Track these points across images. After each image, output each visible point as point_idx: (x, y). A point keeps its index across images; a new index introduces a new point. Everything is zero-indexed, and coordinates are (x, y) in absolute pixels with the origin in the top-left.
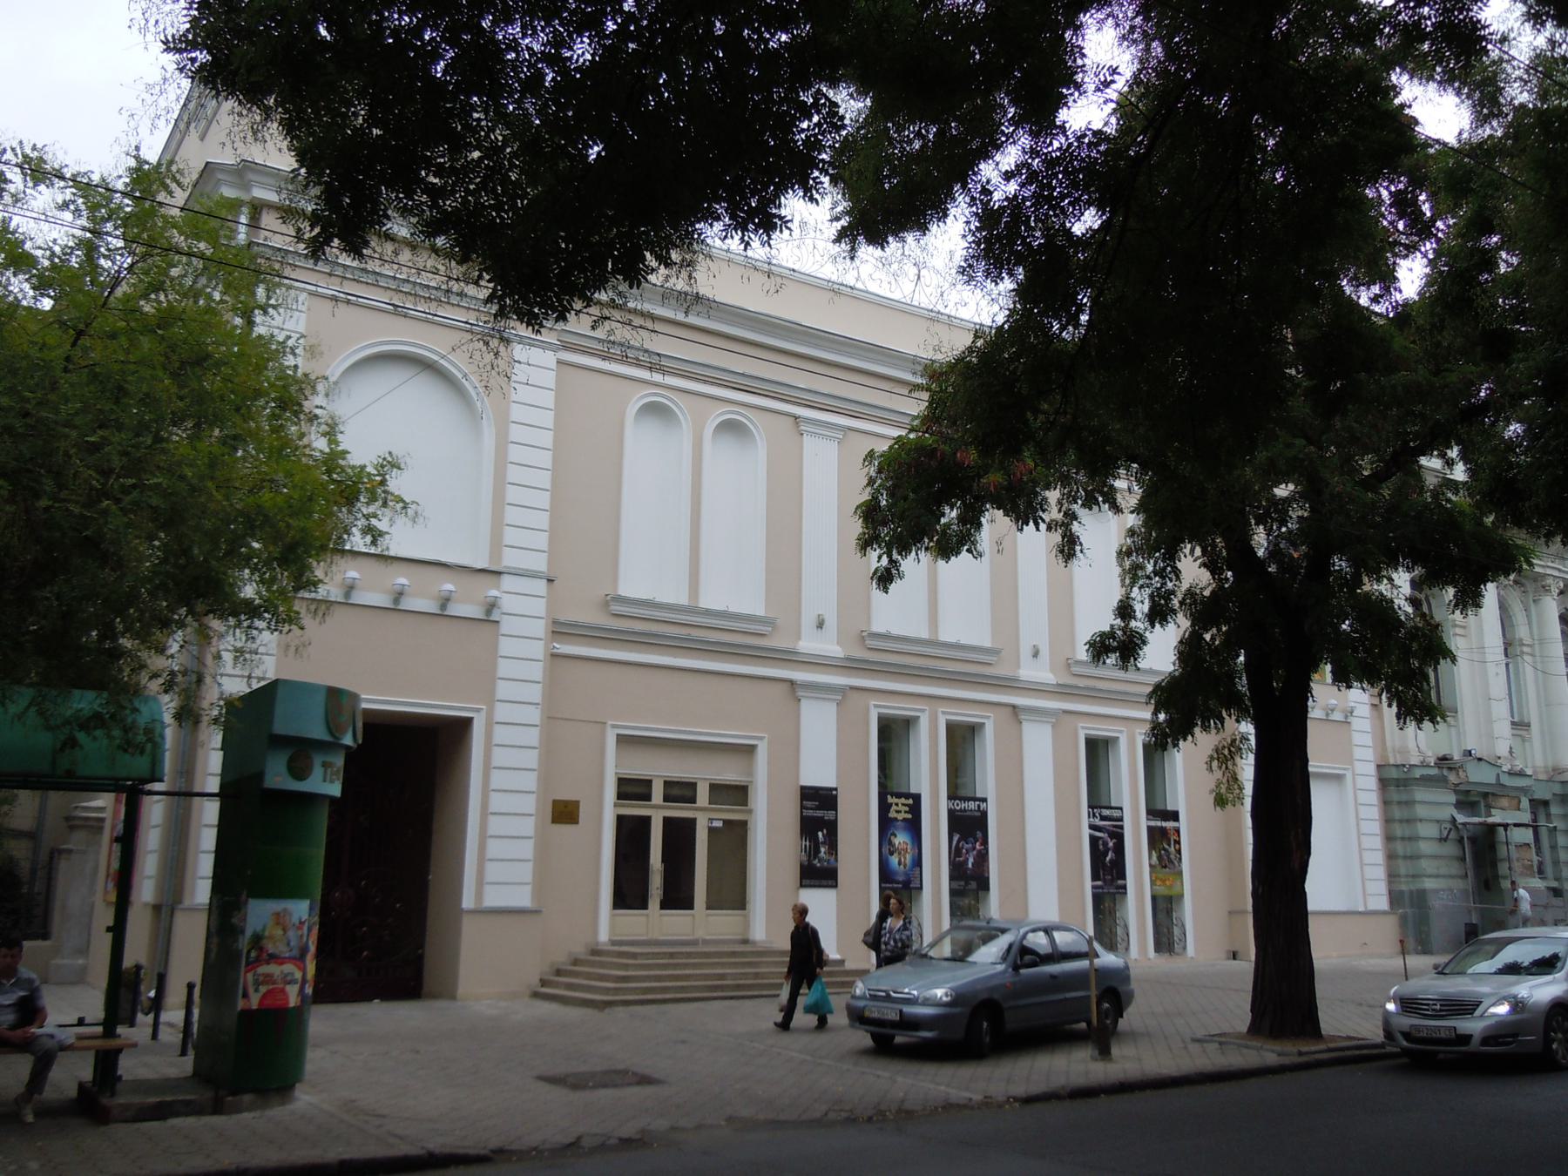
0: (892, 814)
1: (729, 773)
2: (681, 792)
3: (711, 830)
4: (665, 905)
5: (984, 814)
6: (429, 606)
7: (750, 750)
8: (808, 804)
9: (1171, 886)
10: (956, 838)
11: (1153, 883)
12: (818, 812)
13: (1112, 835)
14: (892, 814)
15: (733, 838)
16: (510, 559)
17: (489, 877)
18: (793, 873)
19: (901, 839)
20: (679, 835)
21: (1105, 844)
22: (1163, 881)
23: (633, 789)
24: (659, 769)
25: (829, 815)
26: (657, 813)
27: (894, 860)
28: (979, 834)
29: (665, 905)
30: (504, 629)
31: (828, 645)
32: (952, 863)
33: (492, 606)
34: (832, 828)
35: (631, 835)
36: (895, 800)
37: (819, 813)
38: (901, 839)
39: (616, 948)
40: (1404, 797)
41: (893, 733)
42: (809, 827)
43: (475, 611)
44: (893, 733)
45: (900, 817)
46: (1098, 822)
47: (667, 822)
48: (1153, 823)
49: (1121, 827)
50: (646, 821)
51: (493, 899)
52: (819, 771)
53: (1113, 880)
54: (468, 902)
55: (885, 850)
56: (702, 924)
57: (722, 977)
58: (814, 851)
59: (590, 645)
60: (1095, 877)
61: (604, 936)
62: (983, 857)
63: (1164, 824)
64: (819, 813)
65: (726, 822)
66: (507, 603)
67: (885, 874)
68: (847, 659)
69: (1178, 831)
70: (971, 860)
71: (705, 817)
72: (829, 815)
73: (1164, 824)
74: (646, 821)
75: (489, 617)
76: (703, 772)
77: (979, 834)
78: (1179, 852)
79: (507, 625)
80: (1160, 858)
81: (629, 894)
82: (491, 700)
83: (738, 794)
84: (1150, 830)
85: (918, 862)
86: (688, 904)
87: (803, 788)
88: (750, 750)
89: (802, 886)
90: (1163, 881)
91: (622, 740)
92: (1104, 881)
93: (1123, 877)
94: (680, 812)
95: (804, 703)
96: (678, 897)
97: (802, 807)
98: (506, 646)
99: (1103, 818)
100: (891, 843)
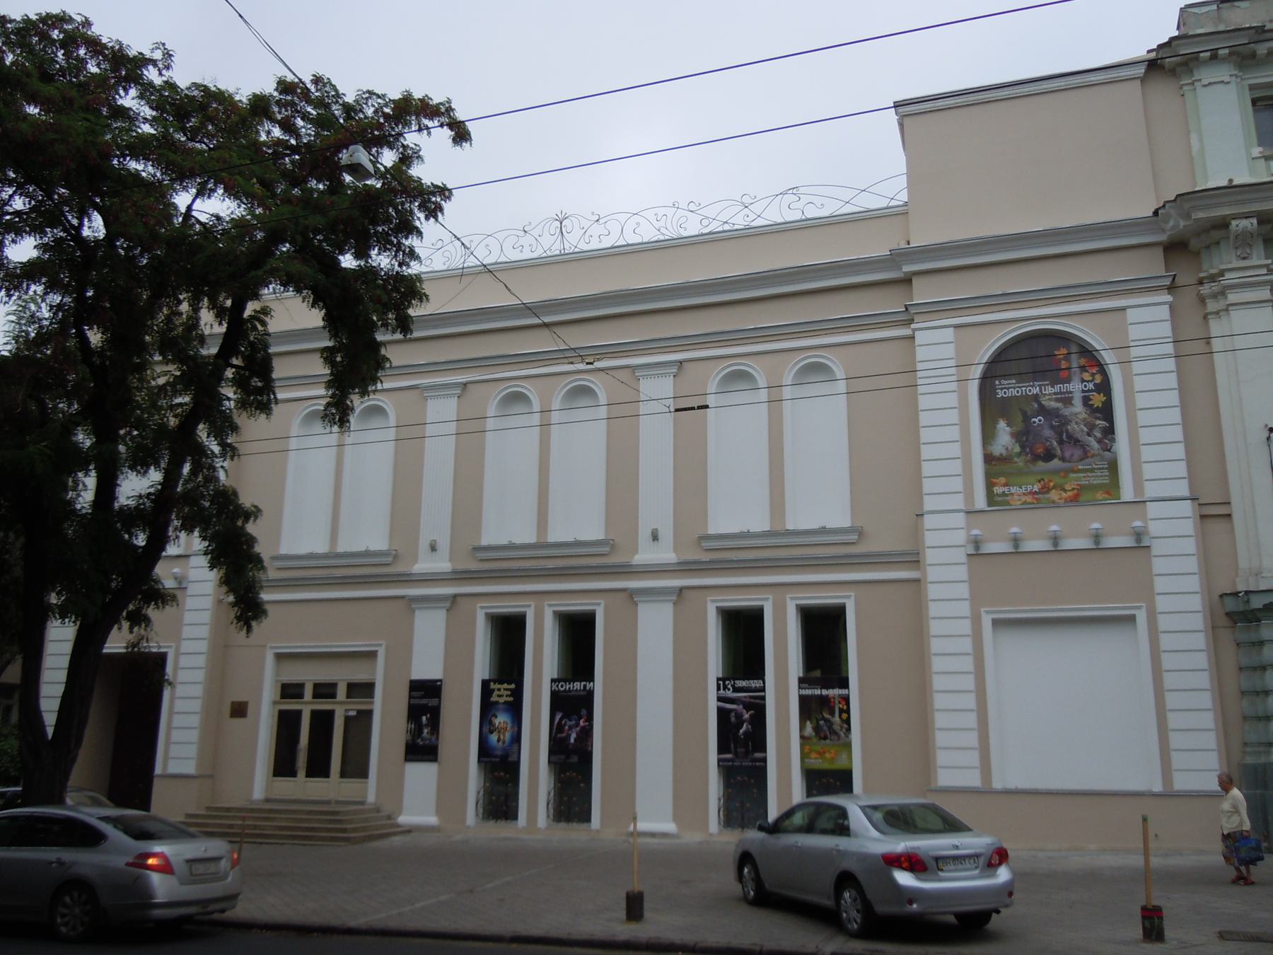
0: (494, 698)
1: (358, 674)
2: (325, 691)
3: (348, 719)
4: (343, 774)
5: (590, 694)
6: (1005, 547)
7: (372, 655)
8: (414, 694)
9: (832, 760)
10: (558, 717)
11: (804, 756)
12: (425, 699)
13: (748, 706)
14: (494, 698)
15: (360, 724)
16: (1151, 490)
17: (172, 754)
18: (401, 750)
19: (501, 719)
20: (323, 722)
21: (739, 716)
22: (821, 754)
23: (290, 691)
24: (309, 675)
25: (432, 702)
26: (307, 707)
27: (494, 738)
28: (584, 712)
29: (309, 774)
30: (1155, 551)
31: (665, 554)
32: (553, 739)
33: (1139, 535)
34: (435, 714)
35: (287, 724)
36: (498, 686)
37: (424, 701)
38: (501, 719)
39: (268, 806)
40: (1253, 637)
41: (509, 632)
42: (414, 713)
43: (1127, 541)
44: (509, 632)
45: (502, 700)
46: (730, 694)
47: (315, 714)
48: (804, 692)
49: (763, 698)
50: (298, 713)
51: (174, 768)
52: (427, 667)
53: (747, 754)
54: (158, 770)
55: (486, 729)
56: (332, 788)
57: (231, 826)
58: (416, 732)
59: (870, 571)
60: (722, 748)
61: (258, 793)
62: (587, 733)
63: (825, 692)
64: (424, 701)
65: (359, 712)
66: (1154, 528)
67: (484, 750)
68: (454, 572)
69: (846, 699)
70: (573, 736)
71: (341, 709)
72: (432, 702)
73: (825, 692)
74: (298, 713)
75: (1140, 544)
76: (341, 675)
77: (584, 712)
78: (848, 721)
79: (1158, 548)
80: (817, 729)
81: (283, 766)
82: (178, 638)
83: (362, 690)
84: (803, 700)
85: (517, 739)
86: (293, 774)
87: (411, 682)
88: (372, 655)
89: (407, 760)
90: (821, 754)
91: (280, 657)
92: (736, 754)
93: (762, 747)
94: (323, 705)
95: (640, 606)
96: (319, 768)
97: (410, 697)
98: (1158, 565)
99: (736, 690)
100: (491, 723)
